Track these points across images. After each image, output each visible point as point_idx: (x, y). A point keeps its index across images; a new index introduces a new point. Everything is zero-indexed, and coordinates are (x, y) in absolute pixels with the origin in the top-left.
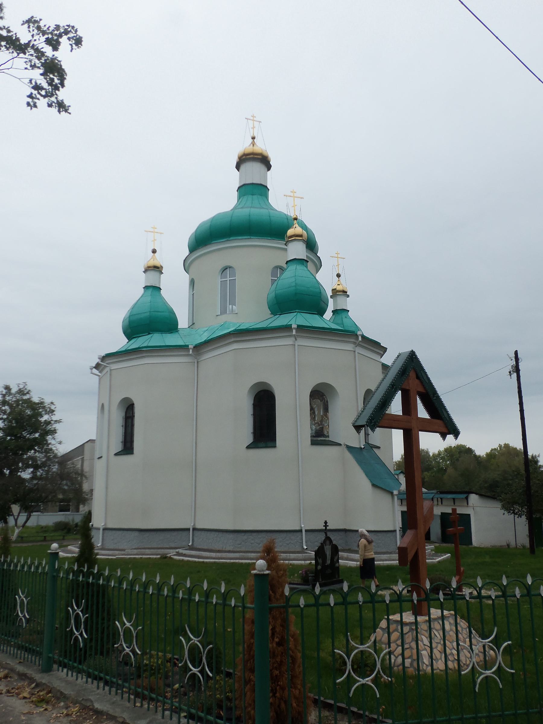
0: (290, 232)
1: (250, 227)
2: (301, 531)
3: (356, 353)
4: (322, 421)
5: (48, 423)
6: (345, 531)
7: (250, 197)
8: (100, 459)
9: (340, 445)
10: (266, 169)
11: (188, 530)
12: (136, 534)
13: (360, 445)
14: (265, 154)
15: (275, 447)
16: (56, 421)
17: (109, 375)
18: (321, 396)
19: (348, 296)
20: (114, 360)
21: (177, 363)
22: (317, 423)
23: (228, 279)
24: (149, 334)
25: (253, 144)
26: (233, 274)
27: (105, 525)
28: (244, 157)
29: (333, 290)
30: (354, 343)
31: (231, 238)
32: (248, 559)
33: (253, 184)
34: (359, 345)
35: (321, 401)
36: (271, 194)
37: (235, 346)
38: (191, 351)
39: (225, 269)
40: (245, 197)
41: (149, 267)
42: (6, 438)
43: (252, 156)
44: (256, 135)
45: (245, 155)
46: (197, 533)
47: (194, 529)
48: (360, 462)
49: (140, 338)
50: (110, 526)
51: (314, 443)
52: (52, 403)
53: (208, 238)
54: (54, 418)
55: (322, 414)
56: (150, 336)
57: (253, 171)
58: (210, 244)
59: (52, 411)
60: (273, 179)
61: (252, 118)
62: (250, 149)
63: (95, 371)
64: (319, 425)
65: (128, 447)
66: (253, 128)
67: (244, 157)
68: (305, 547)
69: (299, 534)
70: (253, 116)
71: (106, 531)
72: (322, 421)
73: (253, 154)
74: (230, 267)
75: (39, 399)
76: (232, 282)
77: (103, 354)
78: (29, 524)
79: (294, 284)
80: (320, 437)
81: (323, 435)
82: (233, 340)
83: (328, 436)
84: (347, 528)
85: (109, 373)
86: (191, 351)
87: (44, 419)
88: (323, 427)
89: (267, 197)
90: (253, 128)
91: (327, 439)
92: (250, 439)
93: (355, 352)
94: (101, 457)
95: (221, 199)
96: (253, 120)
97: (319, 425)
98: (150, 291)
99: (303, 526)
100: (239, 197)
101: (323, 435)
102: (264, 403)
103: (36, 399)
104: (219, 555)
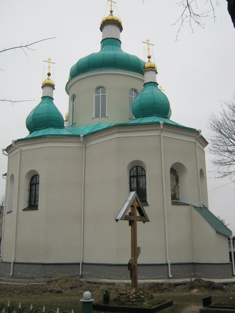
1: (109, 63)
6: (194, 264)
8: (10, 214)
9: (189, 205)
10: (120, 32)
12: (40, 267)
14: (120, 21)
15: (37, 209)
17: (19, 154)
20: (25, 144)
24: (47, 128)
25: (111, 15)
27: (15, 260)
31: (103, 69)
32: (16, 282)
35: (174, 175)
36: (122, 45)
37: (117, 135)
38: (82, 139)
39: (98, 88)
40: (108, 46)
44: (112, 10)
47: (83, 264)
49: (40, 130)
50: (19, 261)
51: (173, 204)
55: (175, 184)
57: (111, 31)
58: (89, 71)
60: (123, 36)
61: (147, 42)
62: (110, 18)
63: (5, 152)
65: (33, 205)
68: (171, 276)
69: (76, 266)
74: (102, 87)
76: (104, 97)
77: (16, 139)
80: (175, 199)
83: (179, 199)
84: (195, 261)
85: (19, 152)
86: (82, 139)
89: (120, 47)
91: (178, 201)
94: (11, 212)
95: (91, 46)
98: (46, 100)
99: (168, 261)
100: (102, 47)
102: (137, 176)
104: (22, 280)
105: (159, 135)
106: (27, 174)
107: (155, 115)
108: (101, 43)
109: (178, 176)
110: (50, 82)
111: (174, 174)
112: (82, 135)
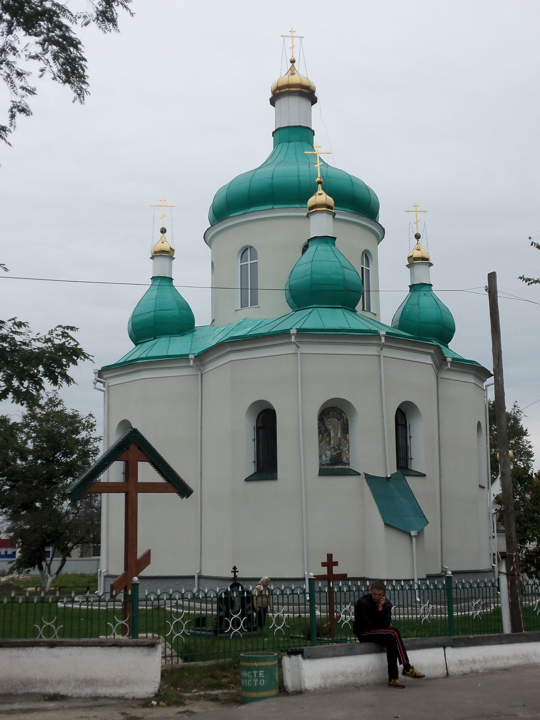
0: (312, 201)
2: (304, 579)
3: (382, 357)
4: (339, 445)
5: (87, 442)
7: (286, 144)
9: (359, 474)
11: (193, 577)
13: (387, 473)
14: (305, 83)
15: (275, 478)
16: (95, 439)
18: (334, 416)
19: (431, 265)
21: (177, 378)
22: (334, 448)
23: (249, 262)
24: (155, 338)
25: (292, 71)
26: (254, 256)
27: (107, 571)
28: (278, 91)
29: (409, 258)
30: (379, 345)
31: (252, 209)
33: (289, 127)
34: (382, 346)
35: (339, 420)
37: (233, 357)
39: (245, 250)
40: (280, 145)
41: (155, 252)
42: (36, 462)
43: (287, 89)
45: (278, 88)
46: (202, 581)
47: (200, 577)
48: (376, 496)
51: (323, 473)
52: (90, 415)
53: (232, 206)
54: (94, 435)
55: (339, 436)
56: (156, 340)
57: (293, 110)
59: (91, 426)
62: (285, 80)
64: (336, 450)
66: (292, 47)
67: (278, 91)
69: (190, 581)
70: (292, 31)
71: (108, 579)
72: (339, 445)
73: (288, 86)
74: (251, 247)
75: (72, 411)
76: (254, 266)
78: (64, 571)
79: (309, 272)
80: (335, 465)
81: (341, 463)
82: (229, 349)
83: (349, 464)
87: (81, 437)
88: (341, 453)
89: (311, 143)
90: (292, 47)
91: (347, 467)
92: (251, 469)
93: (380, 356)
96: (293, 37)
97: (336, 450)
98: (157, 282)
100: (276, 144)
101: (341, 463)
103: (69, 412)
105: (296, 352)
106: (118, 427)
107: (314, 306)
108: (273, 133)
109: (347, 420)
110: (166, 247)
111: (339, 417)
112: (191, 356)
